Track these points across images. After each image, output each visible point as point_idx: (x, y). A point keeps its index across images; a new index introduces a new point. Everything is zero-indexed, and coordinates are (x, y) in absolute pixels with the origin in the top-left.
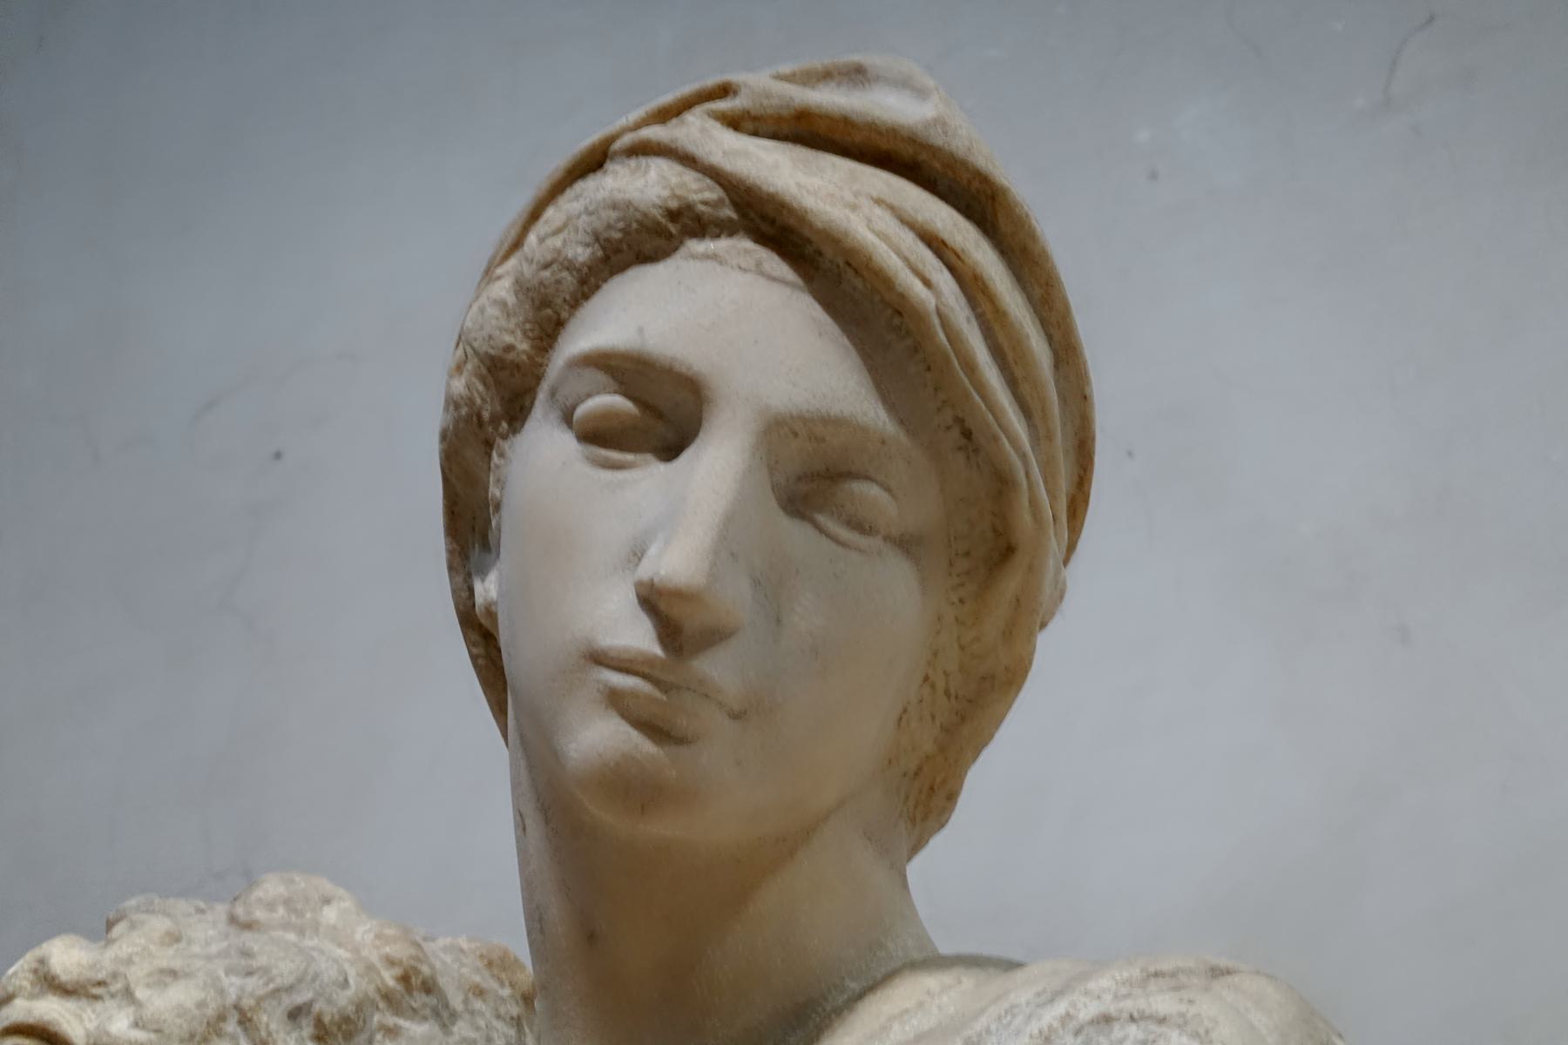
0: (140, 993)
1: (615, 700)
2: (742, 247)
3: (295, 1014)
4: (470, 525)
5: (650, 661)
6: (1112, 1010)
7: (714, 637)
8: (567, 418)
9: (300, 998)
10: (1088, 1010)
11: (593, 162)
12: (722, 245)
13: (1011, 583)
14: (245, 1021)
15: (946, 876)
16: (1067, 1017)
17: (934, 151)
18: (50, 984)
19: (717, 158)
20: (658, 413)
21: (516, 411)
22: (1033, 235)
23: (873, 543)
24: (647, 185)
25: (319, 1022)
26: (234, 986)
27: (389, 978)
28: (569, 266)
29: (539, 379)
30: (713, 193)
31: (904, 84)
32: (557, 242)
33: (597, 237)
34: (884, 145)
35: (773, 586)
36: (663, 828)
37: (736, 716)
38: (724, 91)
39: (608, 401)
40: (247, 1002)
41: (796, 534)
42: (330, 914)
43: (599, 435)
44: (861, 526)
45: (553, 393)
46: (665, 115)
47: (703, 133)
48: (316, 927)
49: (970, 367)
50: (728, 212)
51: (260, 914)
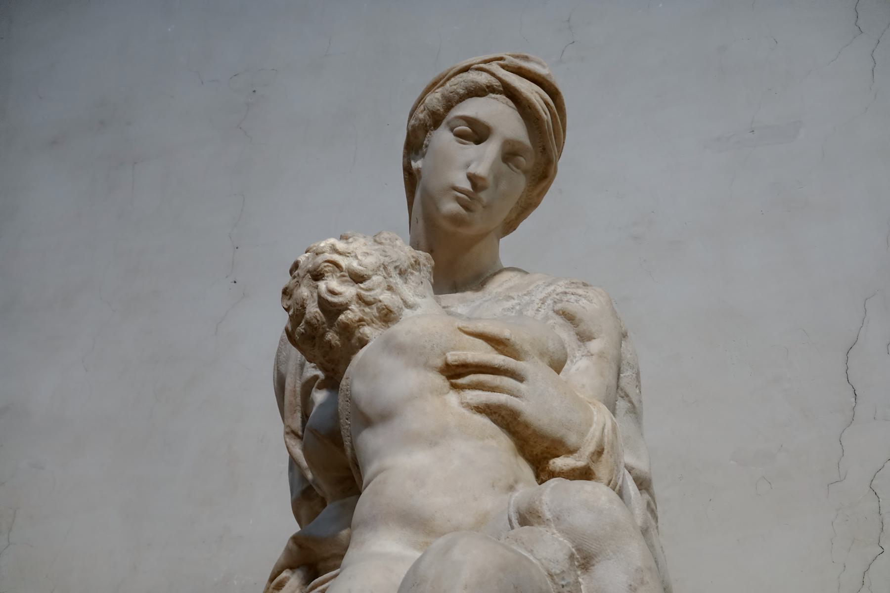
0: (359, 257)
1: (458, 199)
2: (502, 97)
3: (396, 268)
4: (414, 145)
5: (469, 192)
6: (567, 290)
7: (484, 188)
8: (452, 130)
9: (397, 264)
10: (560, 290)
11: (466, 69)
12: (498, 96)
13: (544, 184)
14: (385, 268)
15: (508, 248)
16: (554, 290)
17: (547, 81)
18: (335, 250)
19: (500, 75)
20: (478, 133)
21: (436, 124)
22: (563, 104)
23: (518, 171)
24: (483, 79)
25: (400, 270)
26: (382, 259)
27: (412, 260)
28: (458, 94)
29: (444, 118)
30: (499, 84)
31: (539, 63)
32: (455, 87)
33: (466, 88)
34: (536, 78)
35: (497, 178)
36: (464, 231)
37: (484, 207)
38: (501, 59)
39: (464, 128)
40: (386, 263)
41: (504, 167)
42: (398, 243)
43: (460, 136)
44: (518, 167)
45: (448, 123)
46: (486, 62)
47: (494, 67)
48: (396, 245)
49: (550, 135)
50: (501, 89)
51: (383, 241)
